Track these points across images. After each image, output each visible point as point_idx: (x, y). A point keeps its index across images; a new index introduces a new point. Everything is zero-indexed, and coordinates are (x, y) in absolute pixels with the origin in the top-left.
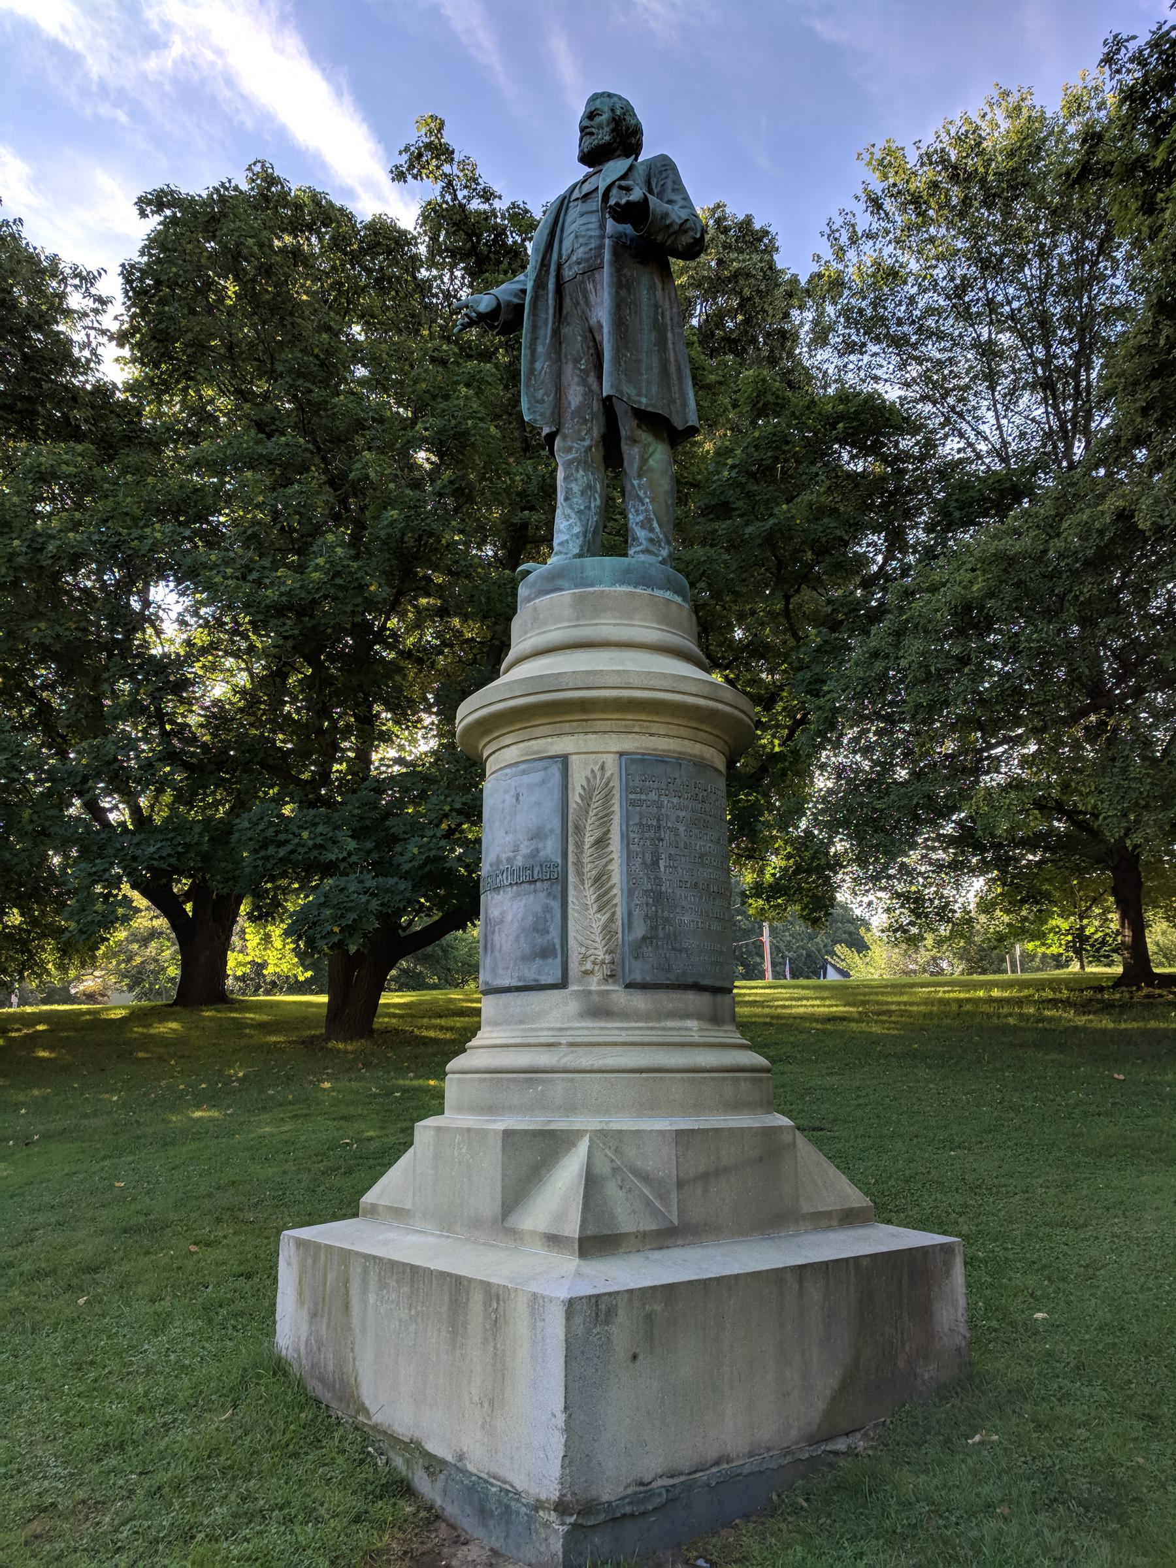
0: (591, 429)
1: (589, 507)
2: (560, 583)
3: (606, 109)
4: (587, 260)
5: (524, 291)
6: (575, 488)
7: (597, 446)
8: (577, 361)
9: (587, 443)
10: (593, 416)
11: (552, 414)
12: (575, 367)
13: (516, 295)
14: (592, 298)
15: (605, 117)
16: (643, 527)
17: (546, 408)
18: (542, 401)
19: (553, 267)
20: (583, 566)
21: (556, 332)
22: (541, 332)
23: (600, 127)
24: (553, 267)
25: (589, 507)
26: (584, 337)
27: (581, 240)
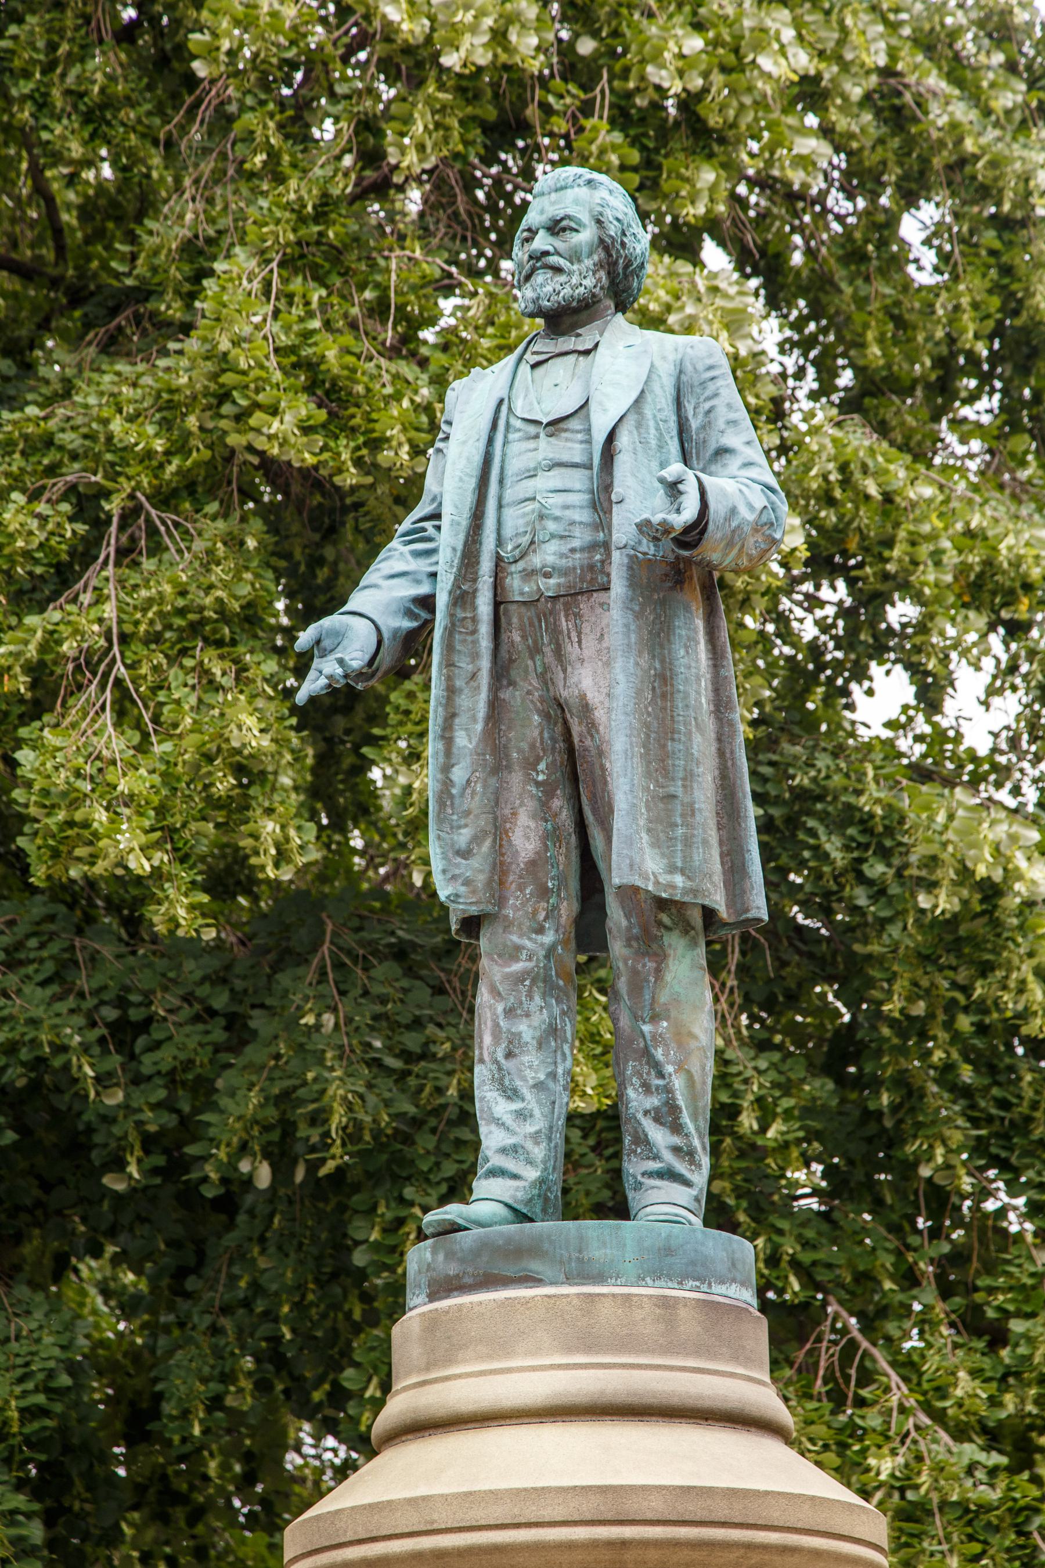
0: (556, 907)
1: (553, 1075)
2: (535, 1266)
3: (585, 218)
4: (565, 572)
5: (427, 602)
6: (526, 1030)
7: (565, 943)
8: (531, 765)
9: (548, 938)
10: (562, 880)
11: (489, 882)
12: (529, 779)
13: (409, 614)
14: (572, 650)
15: (586, 236)
16: (657, 1120)
17: (476, 867)
18: (465, 854)
19: (486, 566)
20: (581, 1238)
21: (495, 706)
22: (463, 701)
23: (575, 257)
24: (486, 566)
25: (553, 1075)
26: (546, 716)
27: (552, 526)
